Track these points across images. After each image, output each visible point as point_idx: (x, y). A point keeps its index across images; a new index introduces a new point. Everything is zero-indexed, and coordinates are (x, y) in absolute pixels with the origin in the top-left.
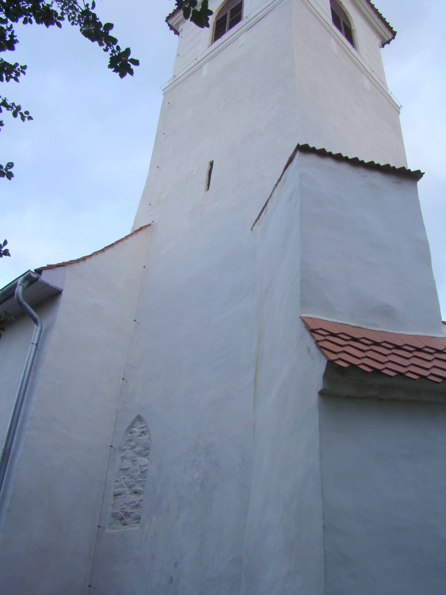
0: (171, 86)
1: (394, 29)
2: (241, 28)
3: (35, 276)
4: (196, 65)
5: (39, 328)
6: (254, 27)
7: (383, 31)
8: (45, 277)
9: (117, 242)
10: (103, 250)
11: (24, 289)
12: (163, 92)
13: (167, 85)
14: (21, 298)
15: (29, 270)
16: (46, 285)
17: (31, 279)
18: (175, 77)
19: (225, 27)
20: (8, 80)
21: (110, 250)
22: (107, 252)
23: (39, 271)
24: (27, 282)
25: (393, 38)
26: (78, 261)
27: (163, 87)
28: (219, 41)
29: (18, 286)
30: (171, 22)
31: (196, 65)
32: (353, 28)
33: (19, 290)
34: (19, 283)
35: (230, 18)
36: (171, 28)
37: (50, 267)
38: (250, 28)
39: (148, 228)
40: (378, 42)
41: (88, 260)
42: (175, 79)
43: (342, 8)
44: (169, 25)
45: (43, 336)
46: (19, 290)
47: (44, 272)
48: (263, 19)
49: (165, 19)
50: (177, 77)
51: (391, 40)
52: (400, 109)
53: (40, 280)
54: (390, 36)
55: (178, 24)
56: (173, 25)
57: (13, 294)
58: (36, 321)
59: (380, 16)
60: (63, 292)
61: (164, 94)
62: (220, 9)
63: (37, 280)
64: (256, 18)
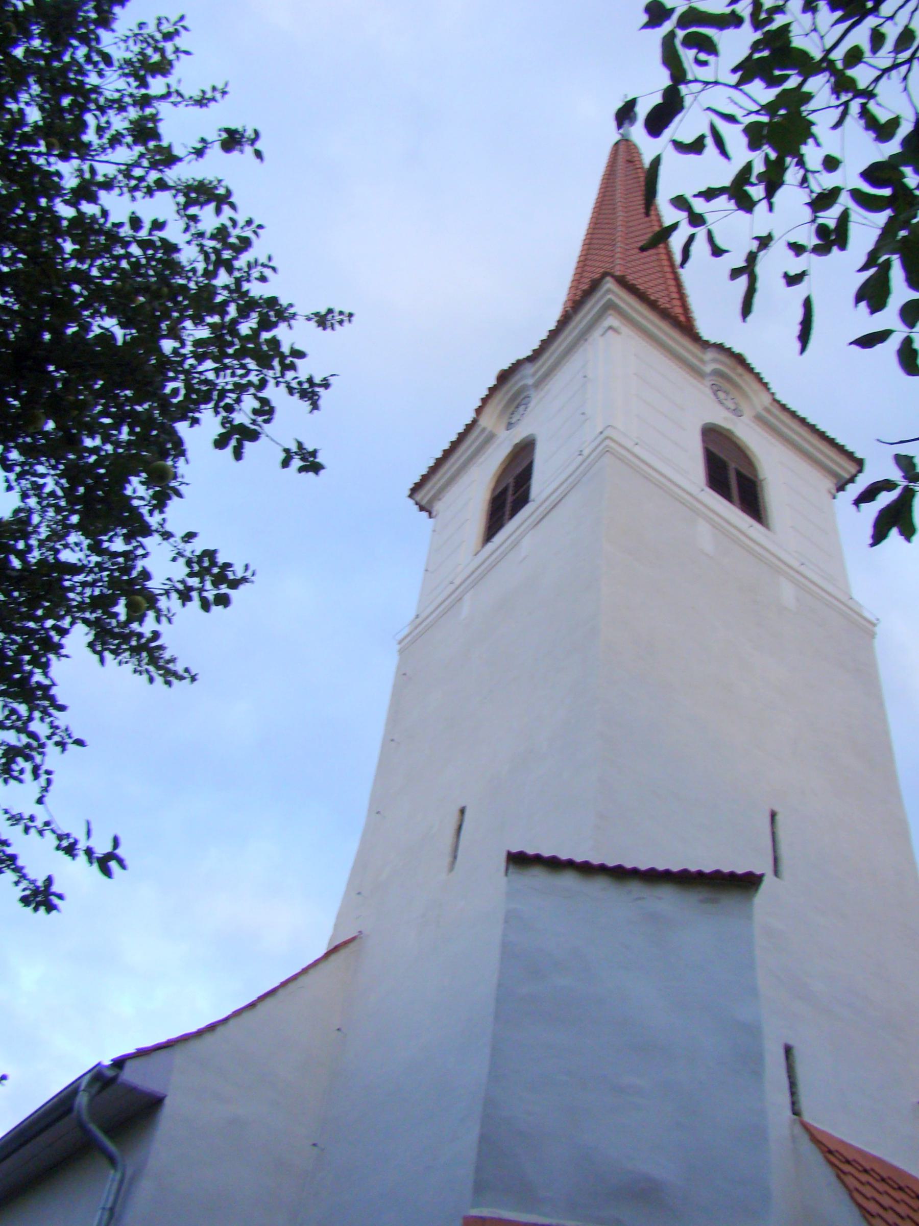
0: (409, 638)
1: (858, 455)
2: (525, 520)
3: (110, 1073)
4: (581, 464)
5: (118, 1176)
6: (545, 520)
7: (832, 460)
8: (129, 1075)
9: (284, 984)
10: (252, 1005)
11: (92, 1099)
12: (398, 647)
13: (405, 632)
14: (85, 1117)
15: (99, 1064)
16: (133, 1090)
17: (103, 1079)
18: (417, 616)
19: (504, 514)
20: (176, 467)
21: (270, 1001)
22: (260, 1007)
23: (119, 1063)
24: (98, 1085)
25: (860, 471)
26: (200, 1033)
27: (400, 637)
28: (491, 546)
29: (81, 1093)
30: (419, 497)
31: (581, 464)
32: (761, 477)
33: (83, 1100)
34: (83, 1087)
35: (514, 494)
36: (422, 509)
37: (142, 1053)
38: (538, 522)
39: (351, 945)
40: (829, 484)
41: (220, 1030)
42: (418, 621)
43: (735, 439)
44: (417, 504)
45: (123, 1192)
46: (83, 1100)
47: (129, 1065)
48: (560, 505)
49: (408, 493)
50: (423, 616)
51: (855, 476)
52: (874, 625)
53: (120, 1080)
54: (853, 469)
55: (431, 501)
56: (423, 503)
57: (70, 1110)
58: (112, 1161)
59: (822, 436)
60: (167, 1102)
61: (401, 652)
62: (499, 472)
63: (113, 1080)
64: (547, 503)
